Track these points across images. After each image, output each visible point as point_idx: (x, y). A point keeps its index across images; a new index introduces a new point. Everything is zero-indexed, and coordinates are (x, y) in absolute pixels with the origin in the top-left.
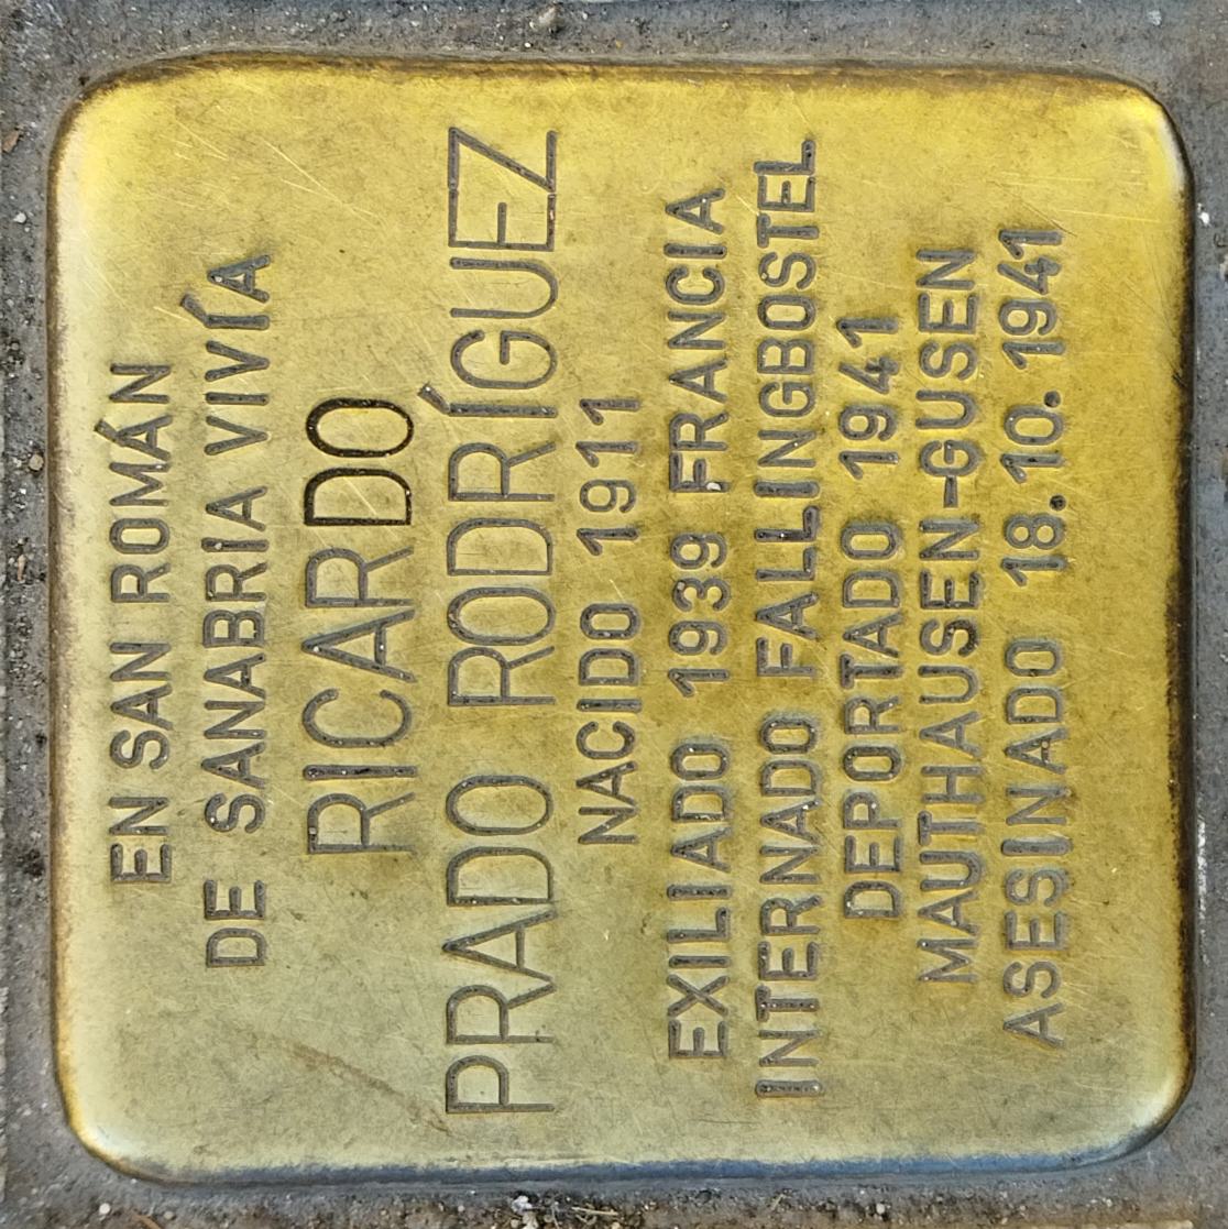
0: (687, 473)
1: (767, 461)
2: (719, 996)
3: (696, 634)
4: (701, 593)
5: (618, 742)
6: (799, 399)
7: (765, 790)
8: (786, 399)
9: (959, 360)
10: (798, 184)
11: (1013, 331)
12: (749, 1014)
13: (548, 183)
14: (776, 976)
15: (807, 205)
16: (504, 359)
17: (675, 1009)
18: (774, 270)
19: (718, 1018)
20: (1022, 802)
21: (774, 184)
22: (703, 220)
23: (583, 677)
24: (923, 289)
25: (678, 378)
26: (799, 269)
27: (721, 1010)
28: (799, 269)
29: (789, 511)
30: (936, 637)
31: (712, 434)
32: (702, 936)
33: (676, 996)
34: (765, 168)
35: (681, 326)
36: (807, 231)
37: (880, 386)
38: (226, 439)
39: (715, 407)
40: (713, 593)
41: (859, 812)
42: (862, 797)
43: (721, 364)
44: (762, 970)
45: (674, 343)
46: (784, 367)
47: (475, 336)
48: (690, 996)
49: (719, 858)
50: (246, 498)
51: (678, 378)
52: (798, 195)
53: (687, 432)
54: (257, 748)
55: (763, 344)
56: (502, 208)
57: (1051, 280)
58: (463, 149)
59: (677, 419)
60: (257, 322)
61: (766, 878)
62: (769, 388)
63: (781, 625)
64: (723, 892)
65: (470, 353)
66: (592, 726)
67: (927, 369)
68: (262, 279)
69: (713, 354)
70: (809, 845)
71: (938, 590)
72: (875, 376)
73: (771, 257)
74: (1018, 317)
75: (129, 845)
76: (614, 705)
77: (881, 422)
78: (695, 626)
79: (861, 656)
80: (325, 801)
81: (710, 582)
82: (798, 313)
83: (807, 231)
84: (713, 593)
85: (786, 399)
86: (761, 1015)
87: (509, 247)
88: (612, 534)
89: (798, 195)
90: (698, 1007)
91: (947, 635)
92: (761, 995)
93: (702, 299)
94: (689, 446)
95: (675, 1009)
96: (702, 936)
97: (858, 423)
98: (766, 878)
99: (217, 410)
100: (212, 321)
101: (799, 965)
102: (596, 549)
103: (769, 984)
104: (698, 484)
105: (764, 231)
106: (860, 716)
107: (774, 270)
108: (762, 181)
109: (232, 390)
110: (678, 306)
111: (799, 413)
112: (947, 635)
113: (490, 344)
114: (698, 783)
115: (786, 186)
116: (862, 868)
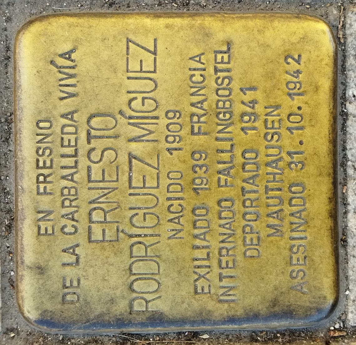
0: (196, 130)
1: (219, 132)
2: (207, 276)
3: (199, 155)
4: (200, 169)
5: (73, 230)
6: (228, 116)
7: (220, 218)
8: (224, 116)
9: (276, 137)
10: (226, 56)
11: (290, 89)
12: (217, 280)
13: (155, 53)
14: (219, 63)
15: (229, 63)
16: (143, 105)
17: (196, 280)
18: (220, 81)
19: (209, 283)
20: (294, 226)
21: (219, 56)
22: (200, 61)
23: (168, 191)
24: (267, 117)
25: (193, 105)
26: (226, 81)
27: (208, 280)
28: (226, 81)
29: (226, 145)
30: (269, 137)
31: (202, 119)
32: (204, 259)
33: (196, 277)
34: (216, 52)
35: (220, 128)
36: (228, 70)
37: (253, 108)
38: (64, 77)
39: (202, 112)
40: (204, 169)
41: (248, 229)
42: (248, 225)
43: (205, 100)
44: (220, 267)
45: (192, 95)
46: (223, 108)
47: (135, 98)
48: (200, 277)
49: (207, 238)
50: (72, 113)
51: (193, 105)
52: (226, 60)
53: (195, 119)
54: (77, 211)
55: (218, 101)
56: (141, 61)
57: (300, 75)
58: (130, 43)
59: (192, 115)
60: (73, 67)
61: (223, 242)
62: (220, 113)
63: (224, 175)
64: (207, 247)
65: (133, 104)
66: (172, 205)
67: (266, 139)
68: (73, 56)
69: (203, 97)
70: (232, 232)
71: (272, 210)
72: (251, 105)
73: (219, 78)
74: (292, 86)
75: (43, 225)
76: (179, 199)
77: (253, 118)
78: (200, 178)
79: (248, 187)
80: (95, 209)
81: (203, 166)
82: (227, 92)
83: (228, 70)
84: (204, 169)
85: (224, 116)
86: (221, 280)
87: (145, 72)
88: (176, 149)
89: (226, 60)
90: (203, 279)
91: (272, 137)
92: (220, 274)
93: (198, 83)
94: (196, 123)
95: (196, 280)
96: (204, 259)
97: (246, 118)
98: (223, 242)
99: (61, 88)
100: (130, 118)
101: (231, 265)
102: (171, 154)
103: (218, 65)
104: (199, 133)
105: (216, 70)
106: (248, 203)
107: (220, 81)
108: (216, 56)
109: (68, 83)
110: (192, 85)
111: (226, 120)
112: (272, 137)
113: (139, 100)
114: (200, 218)
115: (222, 57)
116: (249, 245)
